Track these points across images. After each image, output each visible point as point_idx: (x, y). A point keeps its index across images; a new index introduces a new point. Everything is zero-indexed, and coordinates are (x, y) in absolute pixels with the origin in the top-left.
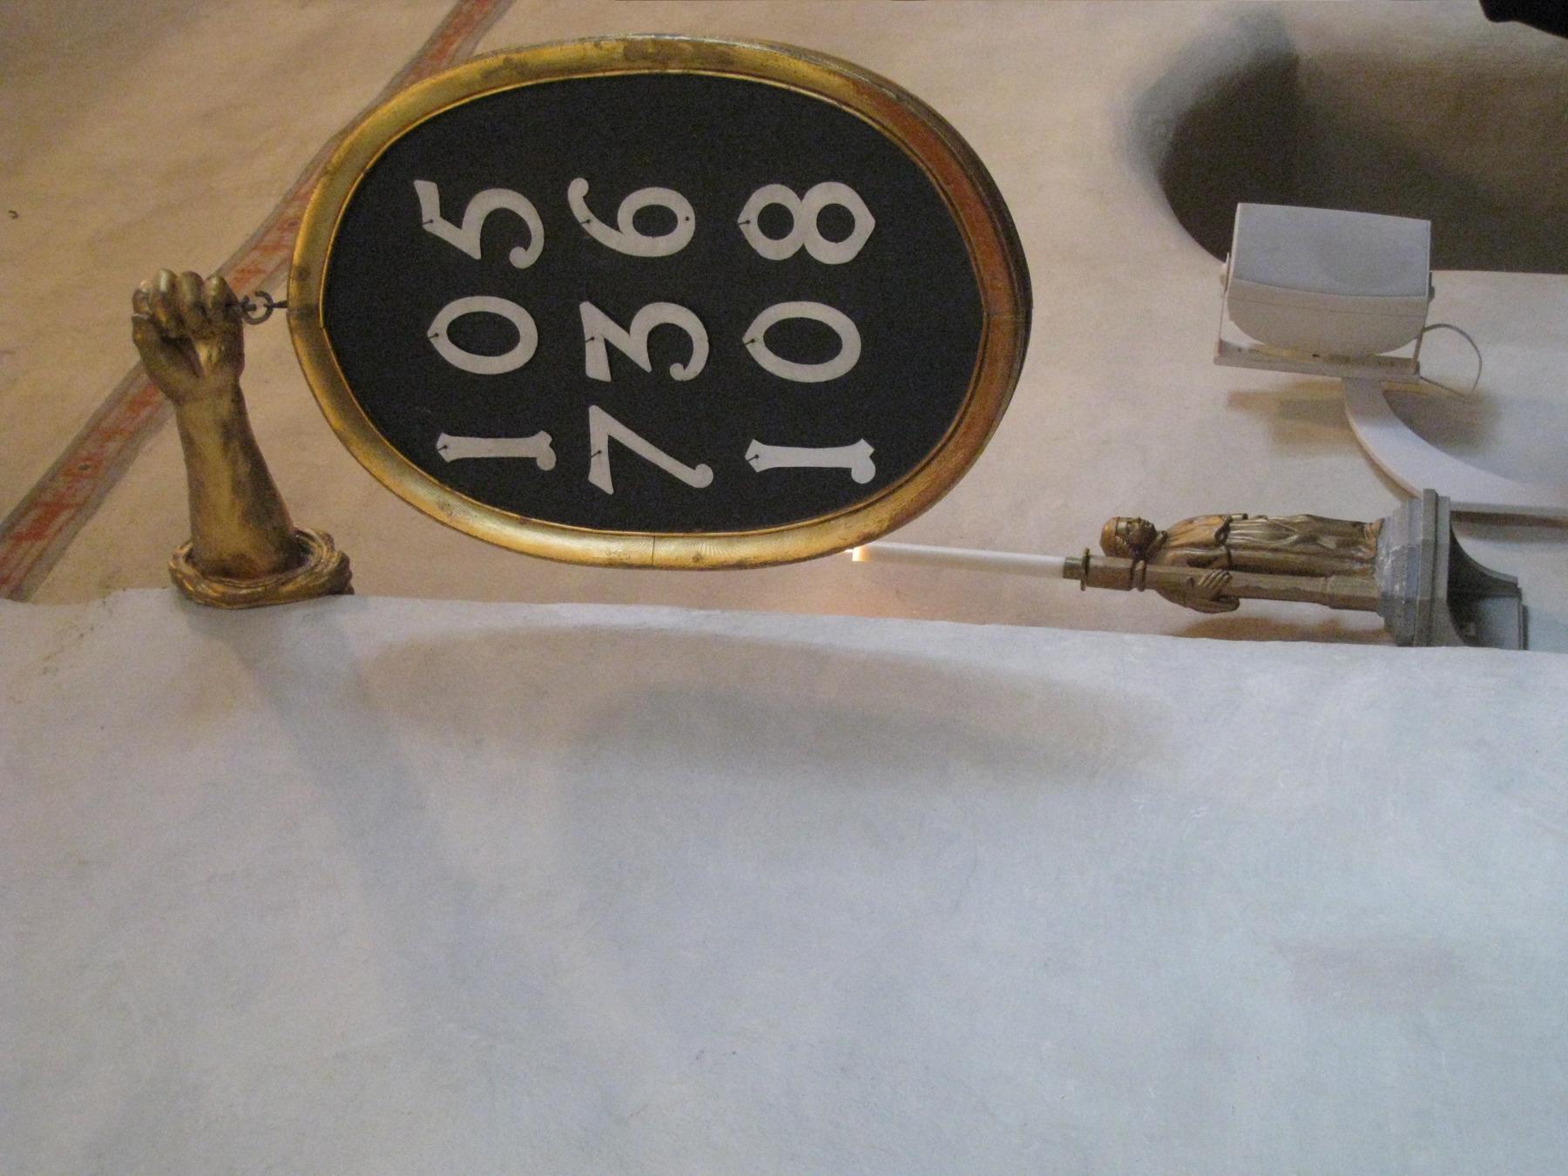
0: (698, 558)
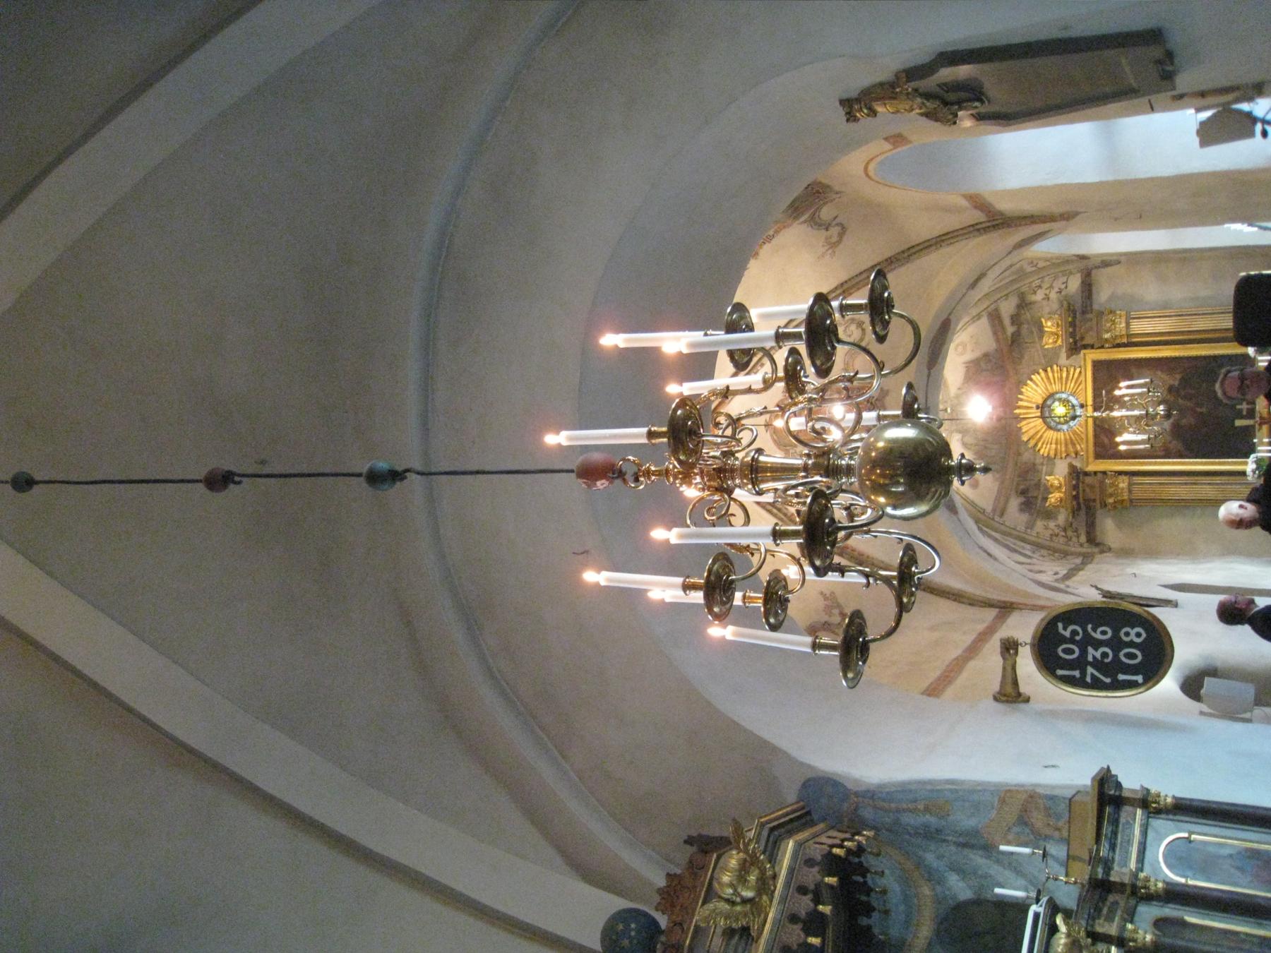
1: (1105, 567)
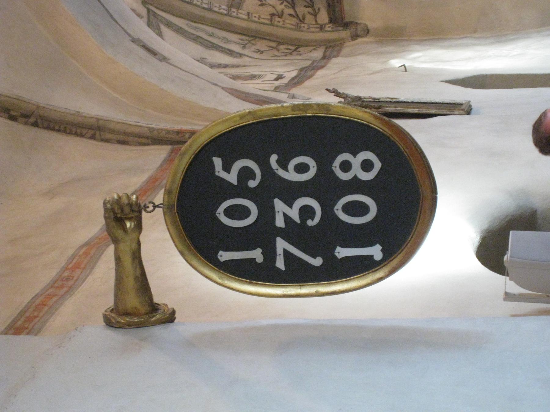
0: (317, 292)
1: (360, 59)
